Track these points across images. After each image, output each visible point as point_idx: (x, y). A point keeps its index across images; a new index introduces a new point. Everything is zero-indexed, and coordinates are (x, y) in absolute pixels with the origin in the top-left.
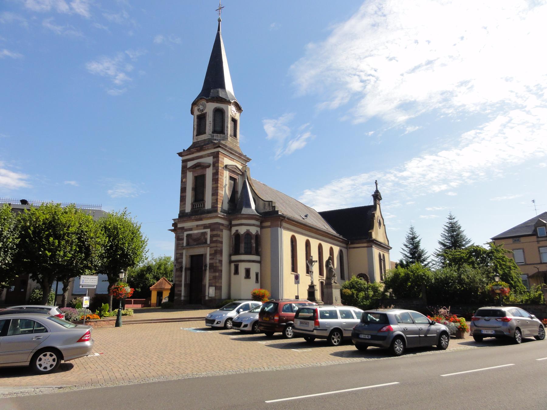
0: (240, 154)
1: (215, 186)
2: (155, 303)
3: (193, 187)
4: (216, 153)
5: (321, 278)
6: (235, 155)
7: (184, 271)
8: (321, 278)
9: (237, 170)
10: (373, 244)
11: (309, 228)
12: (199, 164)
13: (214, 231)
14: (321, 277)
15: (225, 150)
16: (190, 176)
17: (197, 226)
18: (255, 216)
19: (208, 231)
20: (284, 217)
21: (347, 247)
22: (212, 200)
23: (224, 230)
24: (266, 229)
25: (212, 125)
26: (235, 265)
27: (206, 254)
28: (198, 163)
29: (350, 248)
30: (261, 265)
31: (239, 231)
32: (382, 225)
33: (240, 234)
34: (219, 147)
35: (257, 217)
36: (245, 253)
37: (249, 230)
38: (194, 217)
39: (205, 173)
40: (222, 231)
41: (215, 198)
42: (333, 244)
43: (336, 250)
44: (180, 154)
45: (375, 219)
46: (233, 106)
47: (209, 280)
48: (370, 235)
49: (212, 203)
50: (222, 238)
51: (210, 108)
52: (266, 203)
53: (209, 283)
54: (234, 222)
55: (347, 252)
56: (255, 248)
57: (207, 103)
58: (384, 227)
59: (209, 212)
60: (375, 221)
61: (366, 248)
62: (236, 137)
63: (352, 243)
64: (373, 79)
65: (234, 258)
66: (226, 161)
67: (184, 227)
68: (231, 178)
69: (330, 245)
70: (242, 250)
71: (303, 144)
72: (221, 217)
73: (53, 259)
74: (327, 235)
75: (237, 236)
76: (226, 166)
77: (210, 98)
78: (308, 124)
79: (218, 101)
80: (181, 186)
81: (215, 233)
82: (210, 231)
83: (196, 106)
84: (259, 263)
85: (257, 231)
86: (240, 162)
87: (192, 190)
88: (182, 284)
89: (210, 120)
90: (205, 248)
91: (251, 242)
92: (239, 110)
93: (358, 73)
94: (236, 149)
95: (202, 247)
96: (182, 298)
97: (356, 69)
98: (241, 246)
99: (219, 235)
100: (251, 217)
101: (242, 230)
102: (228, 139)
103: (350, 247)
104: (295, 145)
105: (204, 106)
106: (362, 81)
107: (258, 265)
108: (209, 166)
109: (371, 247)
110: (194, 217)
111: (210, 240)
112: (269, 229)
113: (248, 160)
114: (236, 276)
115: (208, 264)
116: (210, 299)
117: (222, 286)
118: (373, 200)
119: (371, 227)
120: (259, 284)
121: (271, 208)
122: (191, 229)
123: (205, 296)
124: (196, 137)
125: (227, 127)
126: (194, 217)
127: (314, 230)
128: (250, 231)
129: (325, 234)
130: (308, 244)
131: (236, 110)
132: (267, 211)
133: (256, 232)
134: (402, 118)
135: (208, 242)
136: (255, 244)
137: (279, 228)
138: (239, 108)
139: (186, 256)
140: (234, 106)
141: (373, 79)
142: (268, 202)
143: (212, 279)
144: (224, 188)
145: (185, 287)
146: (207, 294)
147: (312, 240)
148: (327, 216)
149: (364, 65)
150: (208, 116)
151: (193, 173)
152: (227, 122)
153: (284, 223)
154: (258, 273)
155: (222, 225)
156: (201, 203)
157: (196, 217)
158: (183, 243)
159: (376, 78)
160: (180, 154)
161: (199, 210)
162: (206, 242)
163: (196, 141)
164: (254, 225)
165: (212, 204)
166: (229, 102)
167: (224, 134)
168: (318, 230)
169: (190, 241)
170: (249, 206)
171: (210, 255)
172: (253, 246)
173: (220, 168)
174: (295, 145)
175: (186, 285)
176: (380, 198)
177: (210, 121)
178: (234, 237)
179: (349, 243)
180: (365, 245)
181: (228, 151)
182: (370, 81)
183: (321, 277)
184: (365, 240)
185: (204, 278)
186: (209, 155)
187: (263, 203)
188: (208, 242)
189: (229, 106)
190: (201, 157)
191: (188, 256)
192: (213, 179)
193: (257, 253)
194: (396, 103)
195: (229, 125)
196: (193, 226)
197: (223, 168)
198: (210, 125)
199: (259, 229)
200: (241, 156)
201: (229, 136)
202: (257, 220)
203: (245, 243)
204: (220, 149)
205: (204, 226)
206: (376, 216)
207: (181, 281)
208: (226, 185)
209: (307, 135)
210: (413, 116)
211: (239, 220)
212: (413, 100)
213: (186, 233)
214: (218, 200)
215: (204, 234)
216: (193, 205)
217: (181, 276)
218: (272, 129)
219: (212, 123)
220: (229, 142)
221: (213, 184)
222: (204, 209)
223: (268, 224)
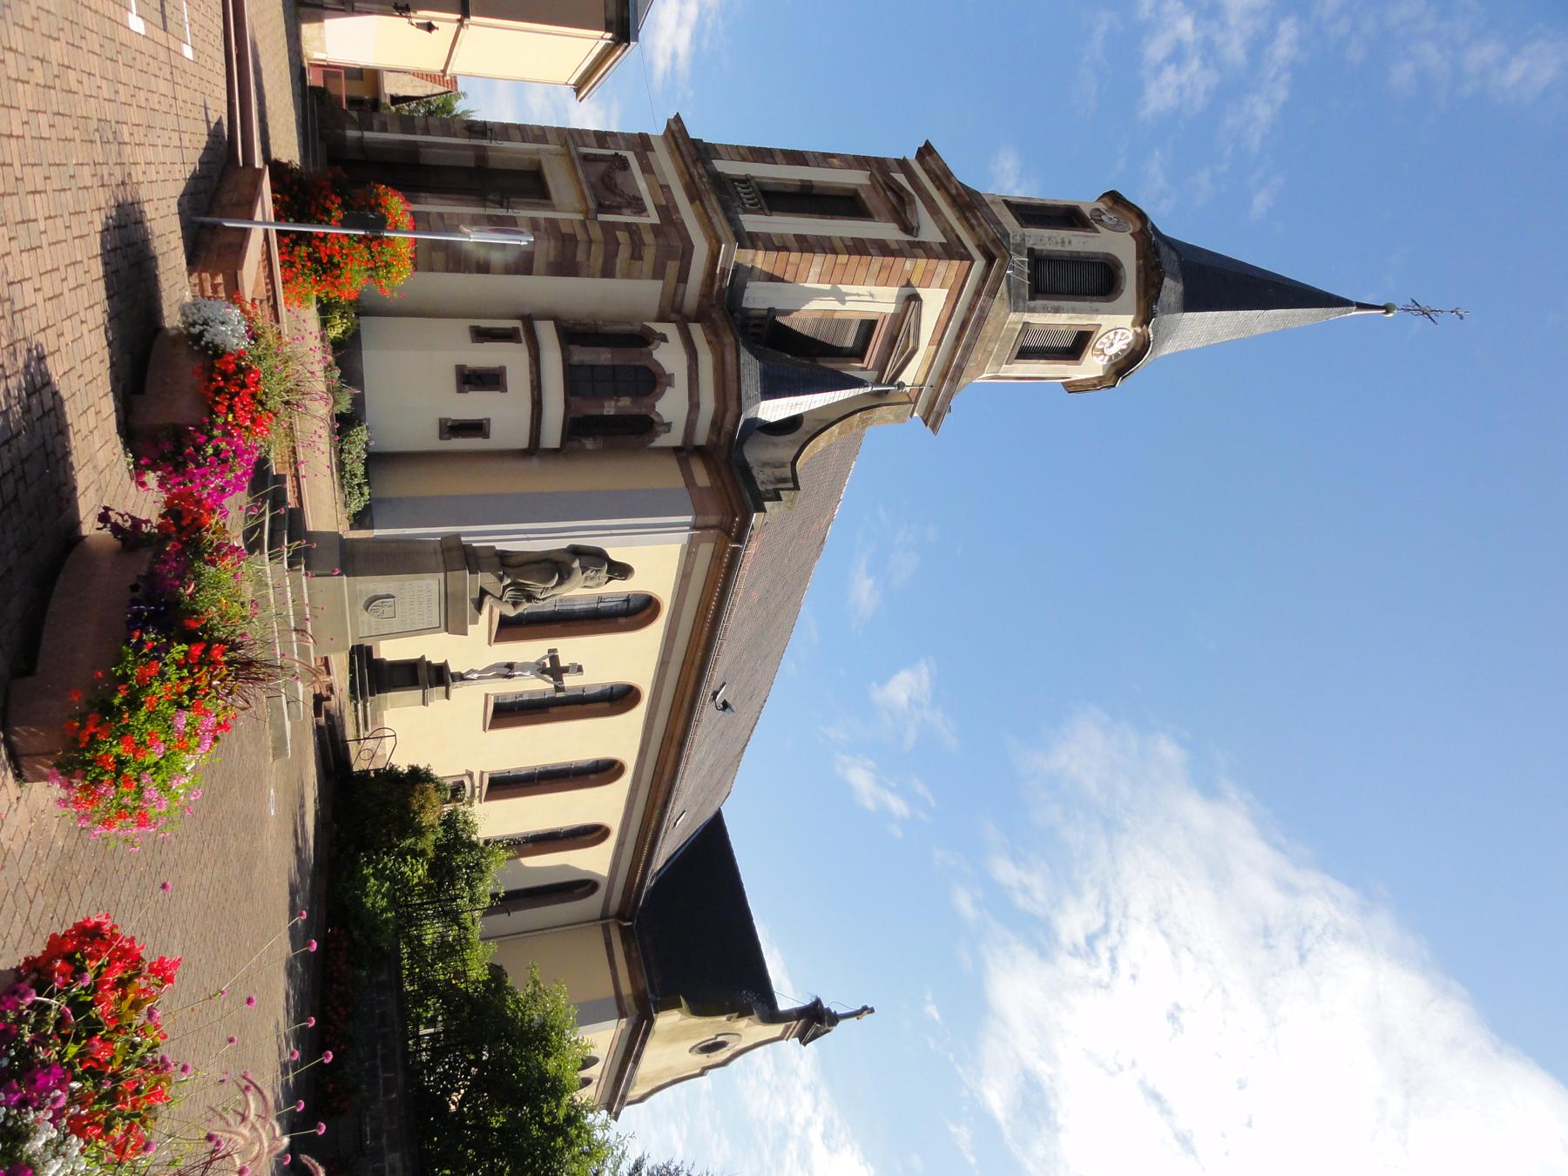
0: (960, 369)
3: (814, 184)
4: (963, 250)
5: (477, 783)
6: (955, 348)
7: (471, 143)
8: (477, 783)
9: (898, 360)
10: (634, 1018)
11: (689, 693)
12: (906, 199)
14: (481, 787)
15: (978, 293)
16: (857, 178)
17: (665, 188)
18: (732, 405)
19: (653, 218)
20: (740, 539)
21: (607, 918)
23: (659, 284)
24: (678, 467)
25: (1059, 248)
27: (553, 208)
29: (606, 929)
32: (704, 1059)
33: (651, 347)
34: (990, 259)
35: (728, 425)
36: (571, 366)
38: (702, 171)
40: (658, 273)
41: (788, 243)
42: (620, 844)
43: (595, 861)
44: (926, 151)
45: (729, 1020)
46: (1131, 337)
48: (669, 1004)
49: (769, 236)
50: (628, 275)
51: (1122, 247)
52: (787, 472)
54: (696, 330)
56: (594, 411)
58: (698, 1071)
59: (733, 222)
60: (723, 1018)
61: (612, 993)
62: (1018, 357)
63: (626, 934)
64: (1102, 973)
65: (547, 333)
66: (934, 301)
68: (868, 327)
69: (614, 821)
70: (583, 355)
71: (869, 804)
72: (716, 265)
74: (660, 802)
75: (643, 340)
76: (915, 298)
77: (1154, 239)
78: (933, 803)
79: (1146, 275)
81: (649, 238)
84: (530, 444)
85: (668, 426)
86: (926, 377)
87: (800, 180)
88: (415, 133)
89: (1074, 241)
90: (578, 206)
91: (617, 394)
92: (1113, 370)
93: (1114, 925)
94: (977, 355)
96: (352, 133)
97: (1125, 915)
98: (603, 349)
99: (641, 258)
100: (729, 395)
101: (669, 356)
102: (1015, 311)
103: (611, 930)
104: (861, 779)
105: (1116, 225)
106: (1091, 940)
107: (522, 442)
108: (908, 228)
109: (622, 1015)
110: (699, 174)
111: (614, 225)
112: (679, 482)
113: (933, 417)
118: (798, 1006)
119: (702, 1008)
120: (434, 443)
121: (770, 487)
122: (647, 169)
125: (1057, 310)
126: (699, 174)
127: (681, 724)
128: (668, 389)
129: (666, 777)
130: (605, 771)
131: (1117, 355)
132: (755, 475)
133: (666, 420)
134: (997, 1097)
135: (602, 217)
136: (612, 413)
137: (689, 519)
138: (1124, 366)
140: (1128, 344)
141: (1102, 973)
142: (790, 475)
144: (828, 287)
145: (403, 142)
147: (619, 790)
148: (713, 838)
149: (1141, 943)
150: (1088, 236)
152: (1074, 311)
153: (712, 545)
154: (486, 435)
155: (683, 277)
156: (759, 202)
159: (1108, 984)
160: (926, 151)
161: (729, 194)
162: (602, 208)
164: (694, 405)
166: (1146, 316)
167: (1032, 298)
168: (681, 745)
170: (772, 390)
172: (606, 404)
173: (909, 264)
174: (861, 779)
176: (810, 1034)
177: (1070, 242)
178: (636, 328)
179: (625, 921)
180: (626, 989)
181: (971, 308)
182: (1096, 967)
183: (481, 787)
184: (644, 983)
186: (946, 230)
187: (786, 460)
189: (1132, 316)
191: (536, 157)
193: (576, 428)
194: (1042, 1068)
195: (1060, 320)
197: (909, 284)
198: (1057, 243)
199: (674, 438)
200: (952, 379)
201: (1027, 317)
202: (717, 425)
203: (614, 367)
204: (979, 264)
205: (671, 205)
206: (742, 1024)
208: (841, 298)
209: (897, 805)
210: (1008, 1136)
211: (709, 343)
212: (1061, 1119)
214: (784, 254)
218: (902, 698)
219: (1063, 249)
220: (1002, 313)
222: (739, 210)
223: (702, 478)
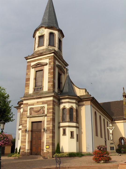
1: (28, 82)
2: (76, 130)
17: (38, 102)
19: (46, 105)
22: (48, 85)
26: (63, 129)
27: (44, 121)
28: (38, 63)
30: (79, 129)
37: (73, 106)
39: (43, 69)
47: (47, 139)
50: (55, 110)
53: (46, 140)
67: (28, 103)
108: (46, 65)
114: (64, 136)
115: (46, 128)
135: (46, 113)
163: (37, 50)
171: (47, 121)
186: (46, 58)
188: (46, 113)
190: (41, 59)
192: (49, 72)
207: (26, 139)
213: (29, 107)
215: (43, 107)
216: (35, 89)
217: (26, 136)
221: (49, 75)
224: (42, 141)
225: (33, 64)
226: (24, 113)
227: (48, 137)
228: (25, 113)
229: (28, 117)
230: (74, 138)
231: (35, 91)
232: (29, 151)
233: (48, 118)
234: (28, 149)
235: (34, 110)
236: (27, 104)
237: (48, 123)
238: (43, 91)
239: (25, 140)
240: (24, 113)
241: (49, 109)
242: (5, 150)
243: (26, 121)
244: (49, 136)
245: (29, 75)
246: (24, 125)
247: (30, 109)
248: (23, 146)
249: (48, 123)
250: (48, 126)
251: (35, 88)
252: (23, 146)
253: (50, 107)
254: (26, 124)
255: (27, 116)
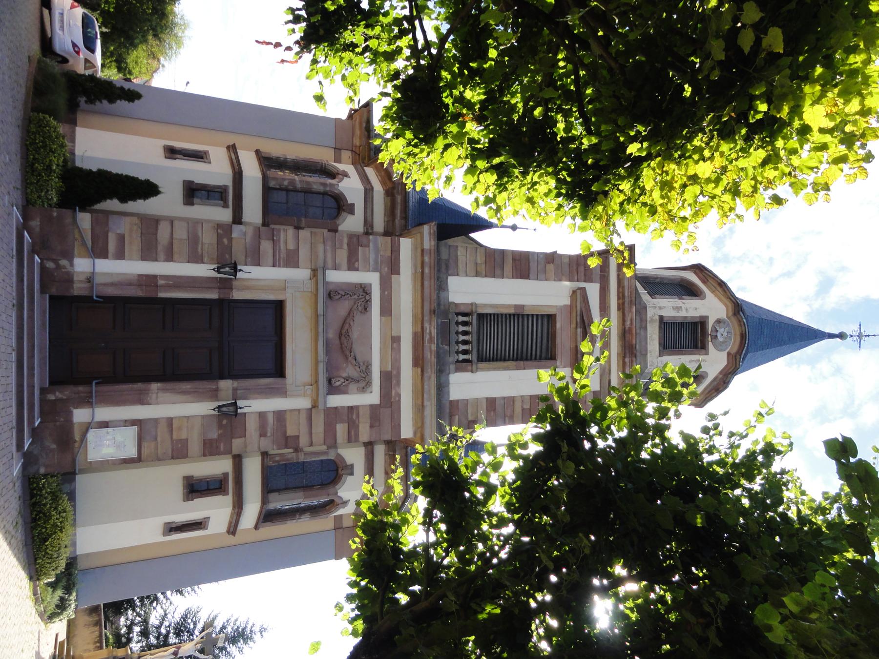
13: (371, 427)
17: (396, 340)
19: (373, 397)
27: (282, 392)
31: (349, 478)
33: (337, 487)
47: (170, 421)
53: (156, 421)
55: (113, 115)
57: (729, 354)
67: (398, 273)
73: (502, 652)
80: (533, 253)
82: (371, 406)
83: (731, 314)
95: (317, 369)
116: (77, 437)
117: (106, 261)
122: (386, 310)
123: (87, 402)
124: (657, 318)
135: (337, 401)
139: (284, 285)
143: (175, 437)
146: (104, 413)
151: (565, 306)
157: (431, 340)
158: (336, 268)
162: (333, 389)
165: (463, 400)
169: (343, 308)
171: (280, 415)
175: (151, 280)
185: (174, 391)
188: (337, 401)
196: (399, 319)
205: (394, 372)
213: (372, 279)
215: (365, 384)
217: (196, 258)
224: (155, 386)
225: (593, 290)
226: (341, 248)
227: (180, 428)
228: (342, 255)
229: (314, 271)
230: (165, 534)
231: (458, 314)
232: (79, 289)
233: (303, 417)
234: (98, 280)
235: (358, 318)
236: (393, 266)
237: (270, 419)
238: (452, 367)
239: (161, 255)
240: (341, 248)
241: (354, 422)
242: (110, 173)
243: (291, 261)
244: (184, 436)
245: (545, 272)
246: (266, 246)
247: (364, 290)
248: (121, 239)
249: (270, 419)
250: (252, 425)
251: (474, 319)
252: (121, 239)
253: (361, 428)
254: (270, 260)
255: (324, 268)
